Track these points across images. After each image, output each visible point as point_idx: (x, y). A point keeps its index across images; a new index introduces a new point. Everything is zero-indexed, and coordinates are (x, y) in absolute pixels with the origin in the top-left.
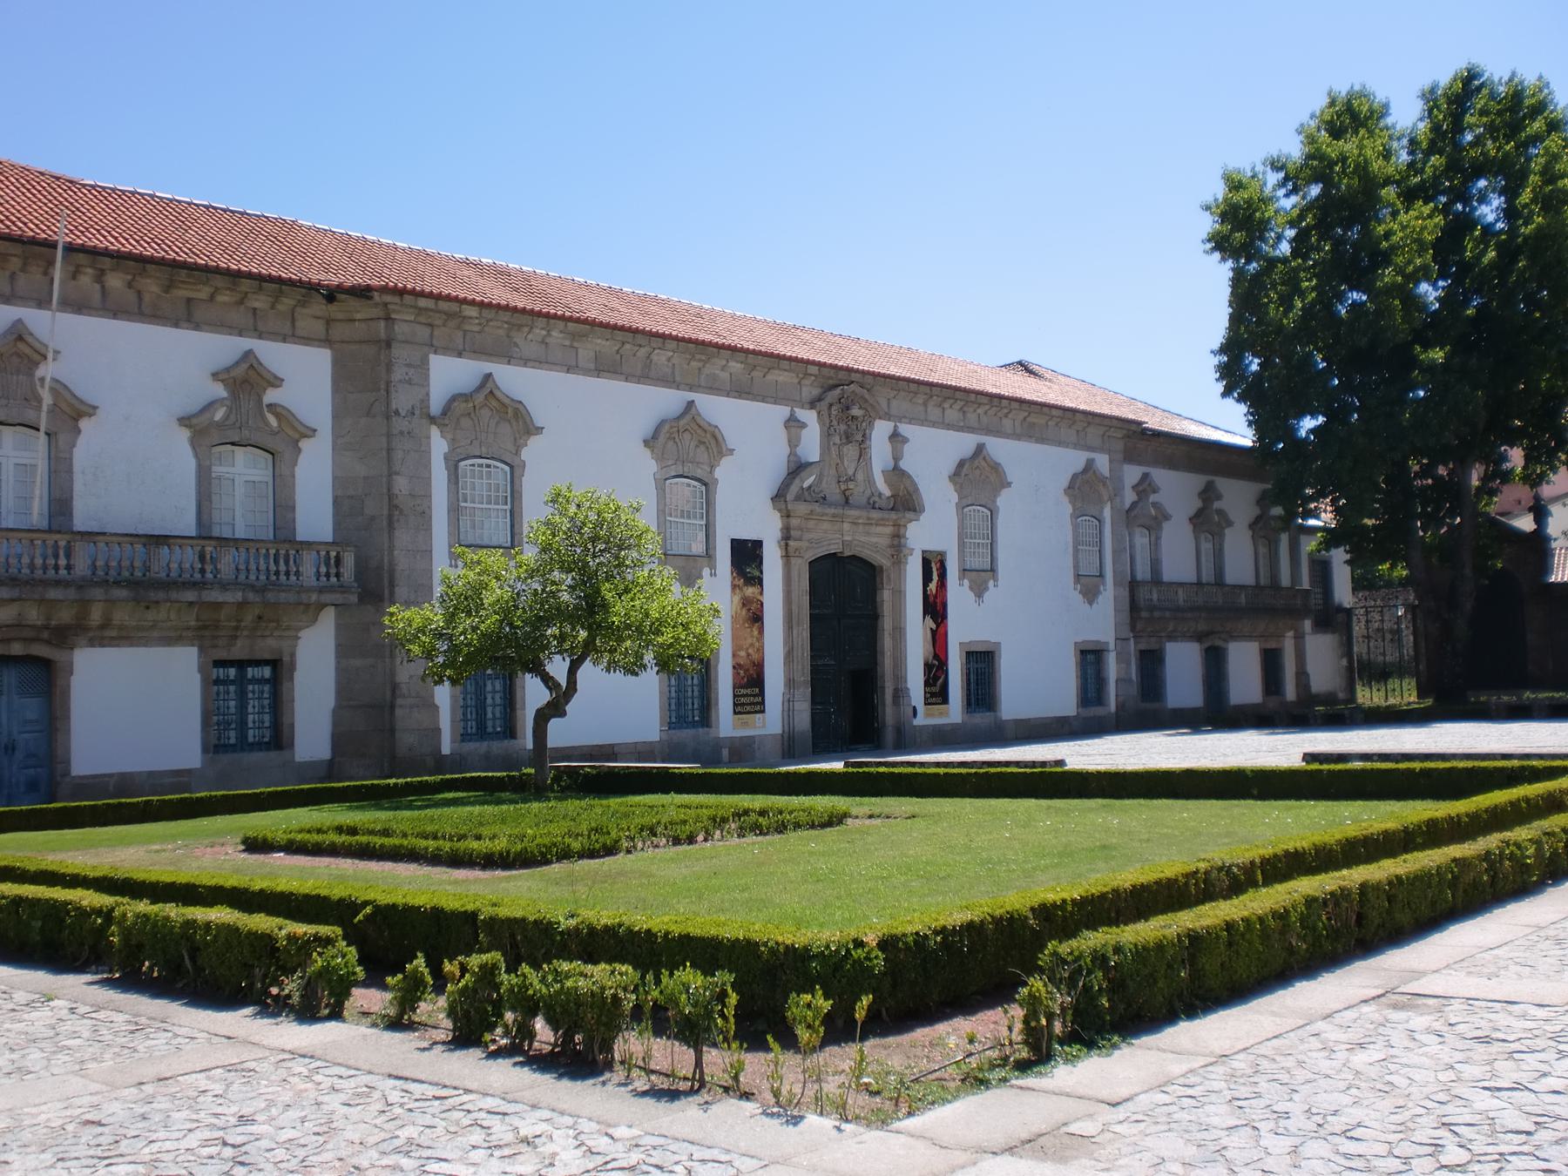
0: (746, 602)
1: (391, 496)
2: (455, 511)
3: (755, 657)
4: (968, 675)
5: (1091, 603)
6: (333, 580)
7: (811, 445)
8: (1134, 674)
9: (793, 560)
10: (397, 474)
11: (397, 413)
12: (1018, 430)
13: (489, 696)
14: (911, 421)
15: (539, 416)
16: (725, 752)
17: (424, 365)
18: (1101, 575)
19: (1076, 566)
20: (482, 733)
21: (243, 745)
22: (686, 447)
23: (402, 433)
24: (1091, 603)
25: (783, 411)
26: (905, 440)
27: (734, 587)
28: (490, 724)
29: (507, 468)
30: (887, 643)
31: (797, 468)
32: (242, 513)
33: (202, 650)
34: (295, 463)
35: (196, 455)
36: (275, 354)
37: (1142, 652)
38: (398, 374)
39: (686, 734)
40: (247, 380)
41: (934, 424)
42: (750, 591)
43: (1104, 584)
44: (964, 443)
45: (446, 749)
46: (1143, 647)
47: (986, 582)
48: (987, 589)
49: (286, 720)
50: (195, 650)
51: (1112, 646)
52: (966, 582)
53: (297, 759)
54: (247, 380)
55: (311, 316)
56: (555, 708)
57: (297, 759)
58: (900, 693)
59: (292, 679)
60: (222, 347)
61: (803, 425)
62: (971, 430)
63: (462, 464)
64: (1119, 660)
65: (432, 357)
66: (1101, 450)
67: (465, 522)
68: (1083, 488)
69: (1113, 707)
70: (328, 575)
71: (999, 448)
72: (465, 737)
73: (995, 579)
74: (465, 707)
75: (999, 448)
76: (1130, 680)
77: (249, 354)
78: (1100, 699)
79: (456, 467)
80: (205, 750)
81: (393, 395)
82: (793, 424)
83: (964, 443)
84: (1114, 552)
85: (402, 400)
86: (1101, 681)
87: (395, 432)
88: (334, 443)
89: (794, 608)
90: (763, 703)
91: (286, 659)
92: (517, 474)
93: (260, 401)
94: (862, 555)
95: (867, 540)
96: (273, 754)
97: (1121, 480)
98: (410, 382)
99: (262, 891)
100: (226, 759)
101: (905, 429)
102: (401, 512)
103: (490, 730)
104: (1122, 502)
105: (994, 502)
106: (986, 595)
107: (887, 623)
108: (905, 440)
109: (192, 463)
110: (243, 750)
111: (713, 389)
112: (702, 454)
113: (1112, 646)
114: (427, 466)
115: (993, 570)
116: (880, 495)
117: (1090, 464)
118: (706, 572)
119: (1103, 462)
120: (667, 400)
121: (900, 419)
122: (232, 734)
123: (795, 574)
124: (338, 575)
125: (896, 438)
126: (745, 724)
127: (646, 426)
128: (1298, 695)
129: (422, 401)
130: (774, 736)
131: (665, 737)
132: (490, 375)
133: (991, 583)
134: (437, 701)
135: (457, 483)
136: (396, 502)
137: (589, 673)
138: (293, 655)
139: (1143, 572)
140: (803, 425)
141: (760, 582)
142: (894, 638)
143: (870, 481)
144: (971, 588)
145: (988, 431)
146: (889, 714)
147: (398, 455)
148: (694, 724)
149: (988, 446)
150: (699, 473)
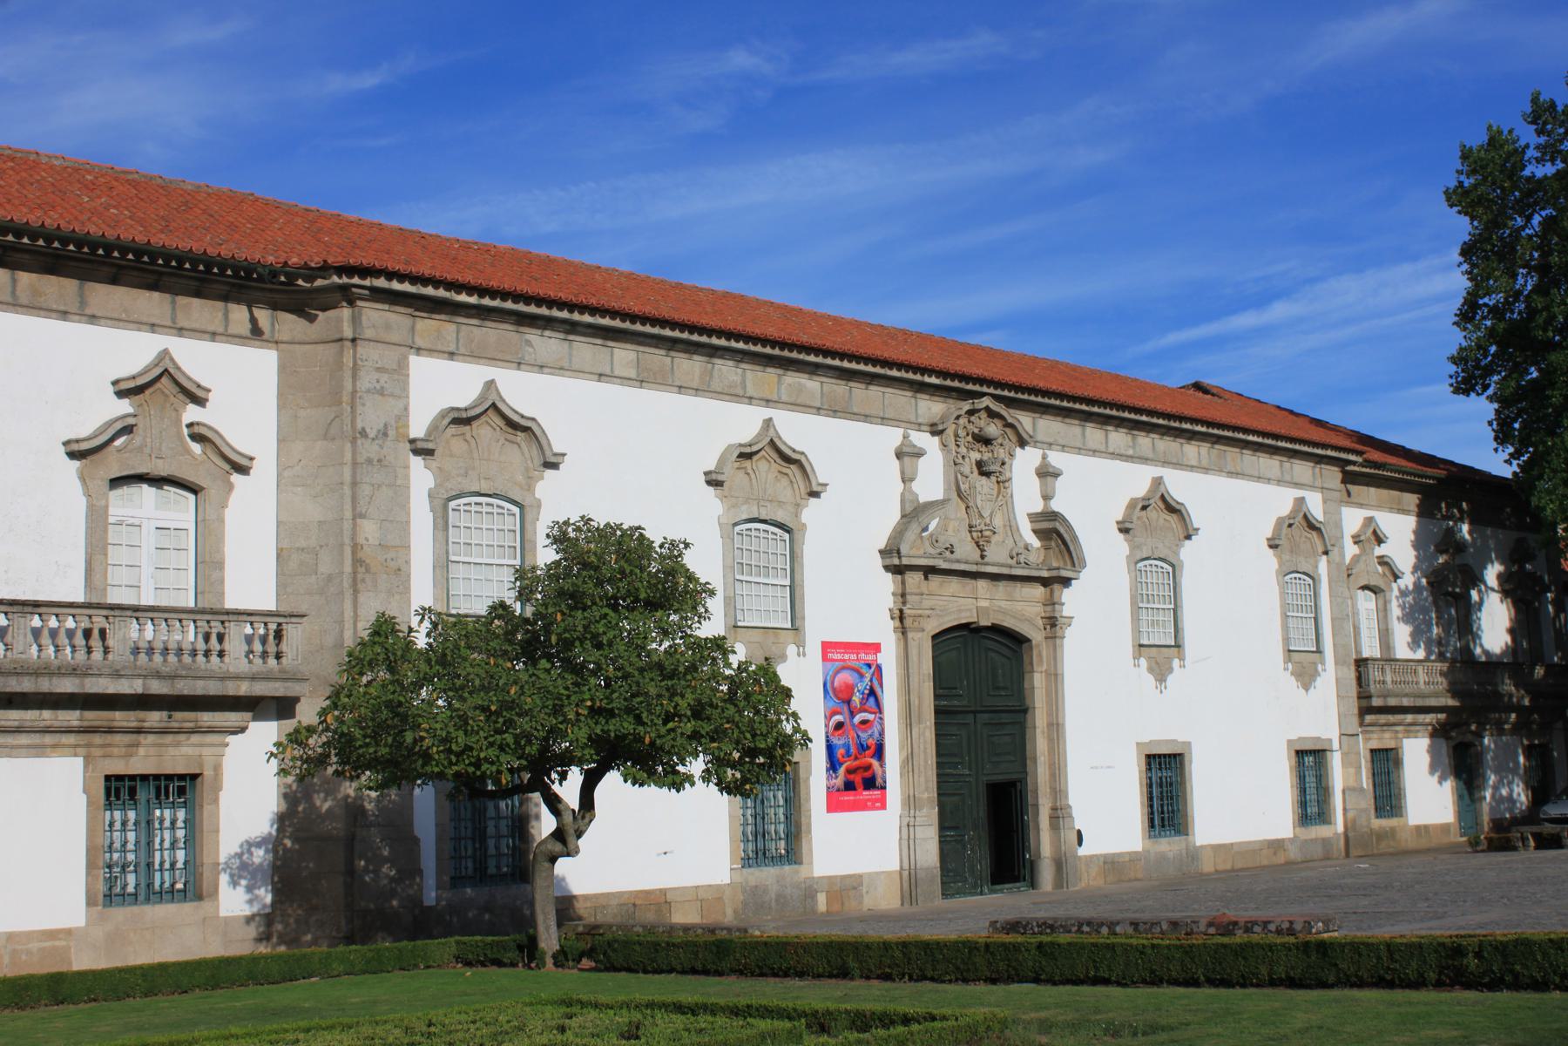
1: (356, 547)
4: (1150, 786)
5: (1307, 688)
6: (272, 662)
7: (931, 481)
8: (1366, 782)
9: (910, 635)
10: (362, 516)
11: (363, 433)
12: (1205, 463)
13: (491, 824)
14: (1063, 448)
17: (402, 369)
18: (1319, 651)
19: (1286, 640)
20: (481, 876)
21: (150, 894)
23: (369, 461)
24: (1307, 688)
25: (892, 436)
26: (1056, 475)
28: (492, 863)
29: (516, 510)
30: (1041, 744)
31: (914, 513)
33: (88, 759)
34: (224, 506)
35: (88, 495)
36: (197, 358)
37: (1372, 751)
38: (367, 381)
41: (1094, 452)
43: (1323, 663)
44: (1135, 480)
45: (430, 896)
46: (1375, 745)
47: (1169, 660)
48: (1171, 670)
50: (79, 762)
51: (1336, 745)
52: (1143, 661)
53: (223, 913)
56: (564, 840)
57: (223, 913)
59: (216, 801)
60: (135, 351)
61: (919, 454)
62: (1144, 460)
63: (452, 504)
64: (1345, 764)
65: (414, 360)
66: (1312, 487)
68: (1299, 535)
69: (1340, 828)
70: (264, 655)
72: (457, 881)
73: (1182, 658)
74: (457, 839)
76: (1362, 789)
77: (165, 354)
78: (1324, 817)
79: (445, 507)
80: (91, 902)
81: (359, 409)
82: (907, 454)
83: (1135, 480)
84: (1333, 620)
85: (371, 416)
86: (1324, 791)
87: (360, 459)
88: (279, 475)
89: (915, 701)
91: (208, 773)
92: (529, 517)
93: (179, 420)
94: (1008, 623)
95: (1016, 608)
96: (188, 907)
97: (1338, 525)
98: (381, 392)
99: (1511, 631)
100: (120, 914)
101: (1056, 459)
102: (368, 571)
103: (492, 870)
104: (1342, 555)
105: (1177, 554)
106: (1170, 679)
107: (1040, 718)
108: (1056, 475)
109: (82, 502)
110: (148, 900)
113: (1336, 745)
114: (405, 506)
115: (1178, 646)
117: (1300, 501)
118: (791, 650)
119: (1316, 505)
120: (741, 422)
122: (131, 879)
123: (913, 652)
124: (278, 656)
125: (1046, 473)
129: (398, 418)
130: (889, 874)
131: (738, 878)
132: (492, 381)
133: (1176, 662)
134: (418, 832)
135: (446, 528)
136: (360, 555)
137: (612, 784)
138: (217, 768)
139: (1371, 649)
140: (919, 454)
142: (1050, 740)
144: (1150, 670)
145: (1166, 463)
146: (1045, 844)
147: (365, 490)
148: (779, 860)
150: (780, 516)
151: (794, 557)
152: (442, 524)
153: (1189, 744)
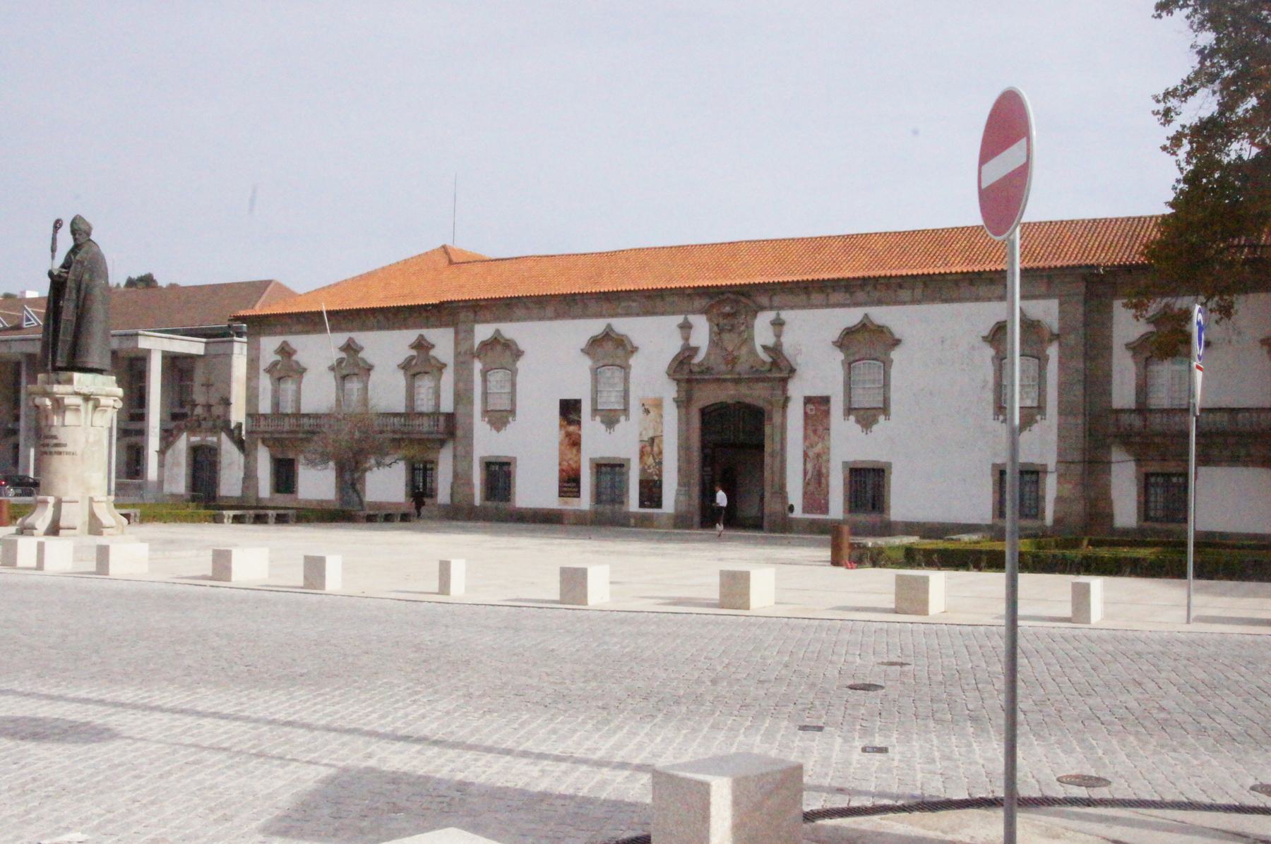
0: (568, 435)
2: (485, 394)
3: (574, 466)
15: (522, 346)
16: (632, 521)
17: (472, 331)
22: (610, 351)
27: (561, 426)
32: (424, 403)
39: (607, 509)
40: (422, 346)
42: (572, 428)
48: (618, 421)
49: (997, 496)
54: (422, 346)
55: (699, 303)
58: (781, 492)
60: (411, 335)
67: (490, 400)
71: (623, 325)
75: (623, 325)
82: (686, 327)
90: (579, 492)
101: (786, 315)
111: (694, 312)
112: (620, 352)
115: (512, 412)
116: (764, 362)
118: (622, 418)
120: (596, 326)
121: (780, 308)
125: (778, 324)
126: (566, 503)
127: (836, 334)
128: (676, 509)
141: (579, 423)
143: (752, 351)
144: (602, 422)
149: (502, 332)
151: (626, 380)
152: (485, 380)
153: (845, 463)
